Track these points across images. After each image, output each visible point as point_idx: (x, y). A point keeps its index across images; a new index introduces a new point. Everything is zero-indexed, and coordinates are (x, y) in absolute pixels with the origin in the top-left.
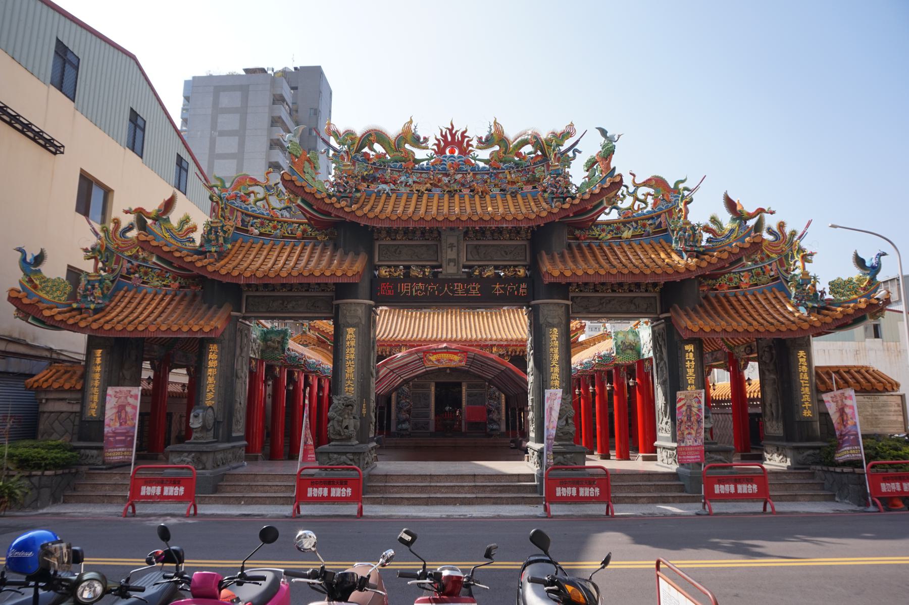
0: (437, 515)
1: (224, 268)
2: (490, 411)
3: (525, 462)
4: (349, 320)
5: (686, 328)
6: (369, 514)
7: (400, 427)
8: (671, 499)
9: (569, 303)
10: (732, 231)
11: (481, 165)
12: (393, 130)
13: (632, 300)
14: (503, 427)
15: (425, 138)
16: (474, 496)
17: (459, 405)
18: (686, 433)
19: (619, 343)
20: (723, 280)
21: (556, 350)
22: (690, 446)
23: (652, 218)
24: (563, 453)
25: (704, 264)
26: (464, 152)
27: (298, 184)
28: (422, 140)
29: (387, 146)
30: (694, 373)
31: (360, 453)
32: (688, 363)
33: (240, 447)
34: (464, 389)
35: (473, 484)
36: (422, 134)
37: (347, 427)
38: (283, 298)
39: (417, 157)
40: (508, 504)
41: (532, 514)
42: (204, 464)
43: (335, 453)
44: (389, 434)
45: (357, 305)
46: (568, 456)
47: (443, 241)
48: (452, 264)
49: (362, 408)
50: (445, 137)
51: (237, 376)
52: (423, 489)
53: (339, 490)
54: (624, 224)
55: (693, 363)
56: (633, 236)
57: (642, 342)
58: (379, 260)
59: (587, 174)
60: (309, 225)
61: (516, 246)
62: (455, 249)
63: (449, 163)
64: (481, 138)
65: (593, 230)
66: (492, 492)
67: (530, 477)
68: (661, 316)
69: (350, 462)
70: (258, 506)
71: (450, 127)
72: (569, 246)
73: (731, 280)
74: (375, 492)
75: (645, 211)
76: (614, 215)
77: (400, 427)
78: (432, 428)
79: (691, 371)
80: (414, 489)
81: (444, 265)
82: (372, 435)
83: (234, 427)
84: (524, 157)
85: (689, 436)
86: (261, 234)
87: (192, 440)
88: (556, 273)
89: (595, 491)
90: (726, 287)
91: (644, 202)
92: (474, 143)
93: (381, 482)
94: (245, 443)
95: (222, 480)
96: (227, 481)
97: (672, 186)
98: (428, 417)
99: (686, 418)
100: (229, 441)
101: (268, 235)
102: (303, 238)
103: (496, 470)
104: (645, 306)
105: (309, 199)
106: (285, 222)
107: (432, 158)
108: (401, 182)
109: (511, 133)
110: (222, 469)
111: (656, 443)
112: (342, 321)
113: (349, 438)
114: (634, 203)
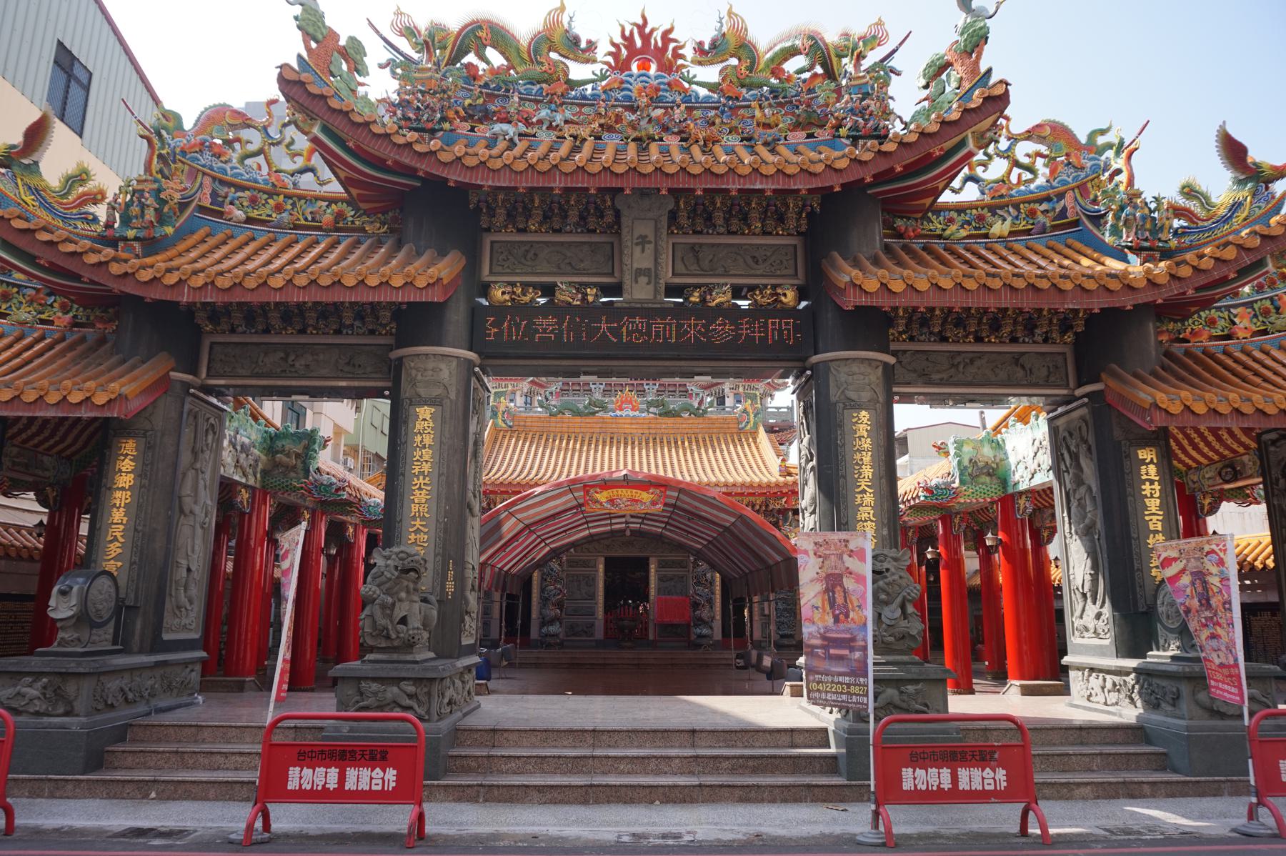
1: (150, 268)
2: (696, 605)
4: (422, 391)
6: (444, 830)
7: (544, 630)
8: (1147, 789)
10: (1236, 206)
11: (703, 92)
12: (524, 24)
13: (1017, 359)
14: (718, 635)
15: (589, 42)
16: (693, 781)
17: (646, 598)
19: (966, 462)
20: (1195, 323)
21: (867, 458)
23: (1048, 199)
25: (1185, 272)
26: (667, 68)
27: (313, 89)
28: (583, 45)
29: (514, 55)
30: (1161, 507)
31: (432, 680)
32: (1147, 486)
33: (186, 664)
34: (653, 568)
35: (689, 752)
36: (584, 33)
37: (403, 621)
40: (773, 801)
42: (70, 703)
43: (374, 679)
44: (527, 643)
45: (441, 362)
46: (911, 688)
47: (625, 231)
50: (629, 40)
51: (182, 511)
52: (576, 765)
53: (365, 773)
54: (993, 209)
55: (1157, 487)
56: (1011, 233)
57: (1012, 460)
58: (491, 273)
61: (777, 248)
62: (650, 248)
63: (637, 86)
64: (701, 43)
65: (930, 221)
66: (733, 771)
67: (819, 736)
68: (1078, 392)
69: (408, 702)
71: (640, 22)
72: (887, 249)
73: (1212, 322)
74: (466, 771)
75: (1032, 186)
76: (971, 193)
78: (599, 633)
79: (1153, 504)
80: (558, 764)
81: (627, 286)
82: (467, 641)
83: (168, 619)
84: (789, 79)
85: (1214, 643)
86: (249, 220)
87: (54, 648)
88: (872, 285)
89: (996, 777)
90: (1205, 336)
91: (1030, 169)
92: (688, 52)
93: (481, 745)
94: (204, 654)
95: (122, 739)
96: (134, 741)
97: (1083, 140)
98: (592, 614)
99: (1195, 603)
100: (153, 650)
101: (263, 222)
102: (337, 230)
103: (739, 720)
104: (1044, 372)
105: (338, 123)
106: (300, 197)
107: (603, 77)
108: (540, 122)
109: (766, 36)
110: (122, 715)
111: (1066, 660)
112: (406, 391)
113: (409, 645)
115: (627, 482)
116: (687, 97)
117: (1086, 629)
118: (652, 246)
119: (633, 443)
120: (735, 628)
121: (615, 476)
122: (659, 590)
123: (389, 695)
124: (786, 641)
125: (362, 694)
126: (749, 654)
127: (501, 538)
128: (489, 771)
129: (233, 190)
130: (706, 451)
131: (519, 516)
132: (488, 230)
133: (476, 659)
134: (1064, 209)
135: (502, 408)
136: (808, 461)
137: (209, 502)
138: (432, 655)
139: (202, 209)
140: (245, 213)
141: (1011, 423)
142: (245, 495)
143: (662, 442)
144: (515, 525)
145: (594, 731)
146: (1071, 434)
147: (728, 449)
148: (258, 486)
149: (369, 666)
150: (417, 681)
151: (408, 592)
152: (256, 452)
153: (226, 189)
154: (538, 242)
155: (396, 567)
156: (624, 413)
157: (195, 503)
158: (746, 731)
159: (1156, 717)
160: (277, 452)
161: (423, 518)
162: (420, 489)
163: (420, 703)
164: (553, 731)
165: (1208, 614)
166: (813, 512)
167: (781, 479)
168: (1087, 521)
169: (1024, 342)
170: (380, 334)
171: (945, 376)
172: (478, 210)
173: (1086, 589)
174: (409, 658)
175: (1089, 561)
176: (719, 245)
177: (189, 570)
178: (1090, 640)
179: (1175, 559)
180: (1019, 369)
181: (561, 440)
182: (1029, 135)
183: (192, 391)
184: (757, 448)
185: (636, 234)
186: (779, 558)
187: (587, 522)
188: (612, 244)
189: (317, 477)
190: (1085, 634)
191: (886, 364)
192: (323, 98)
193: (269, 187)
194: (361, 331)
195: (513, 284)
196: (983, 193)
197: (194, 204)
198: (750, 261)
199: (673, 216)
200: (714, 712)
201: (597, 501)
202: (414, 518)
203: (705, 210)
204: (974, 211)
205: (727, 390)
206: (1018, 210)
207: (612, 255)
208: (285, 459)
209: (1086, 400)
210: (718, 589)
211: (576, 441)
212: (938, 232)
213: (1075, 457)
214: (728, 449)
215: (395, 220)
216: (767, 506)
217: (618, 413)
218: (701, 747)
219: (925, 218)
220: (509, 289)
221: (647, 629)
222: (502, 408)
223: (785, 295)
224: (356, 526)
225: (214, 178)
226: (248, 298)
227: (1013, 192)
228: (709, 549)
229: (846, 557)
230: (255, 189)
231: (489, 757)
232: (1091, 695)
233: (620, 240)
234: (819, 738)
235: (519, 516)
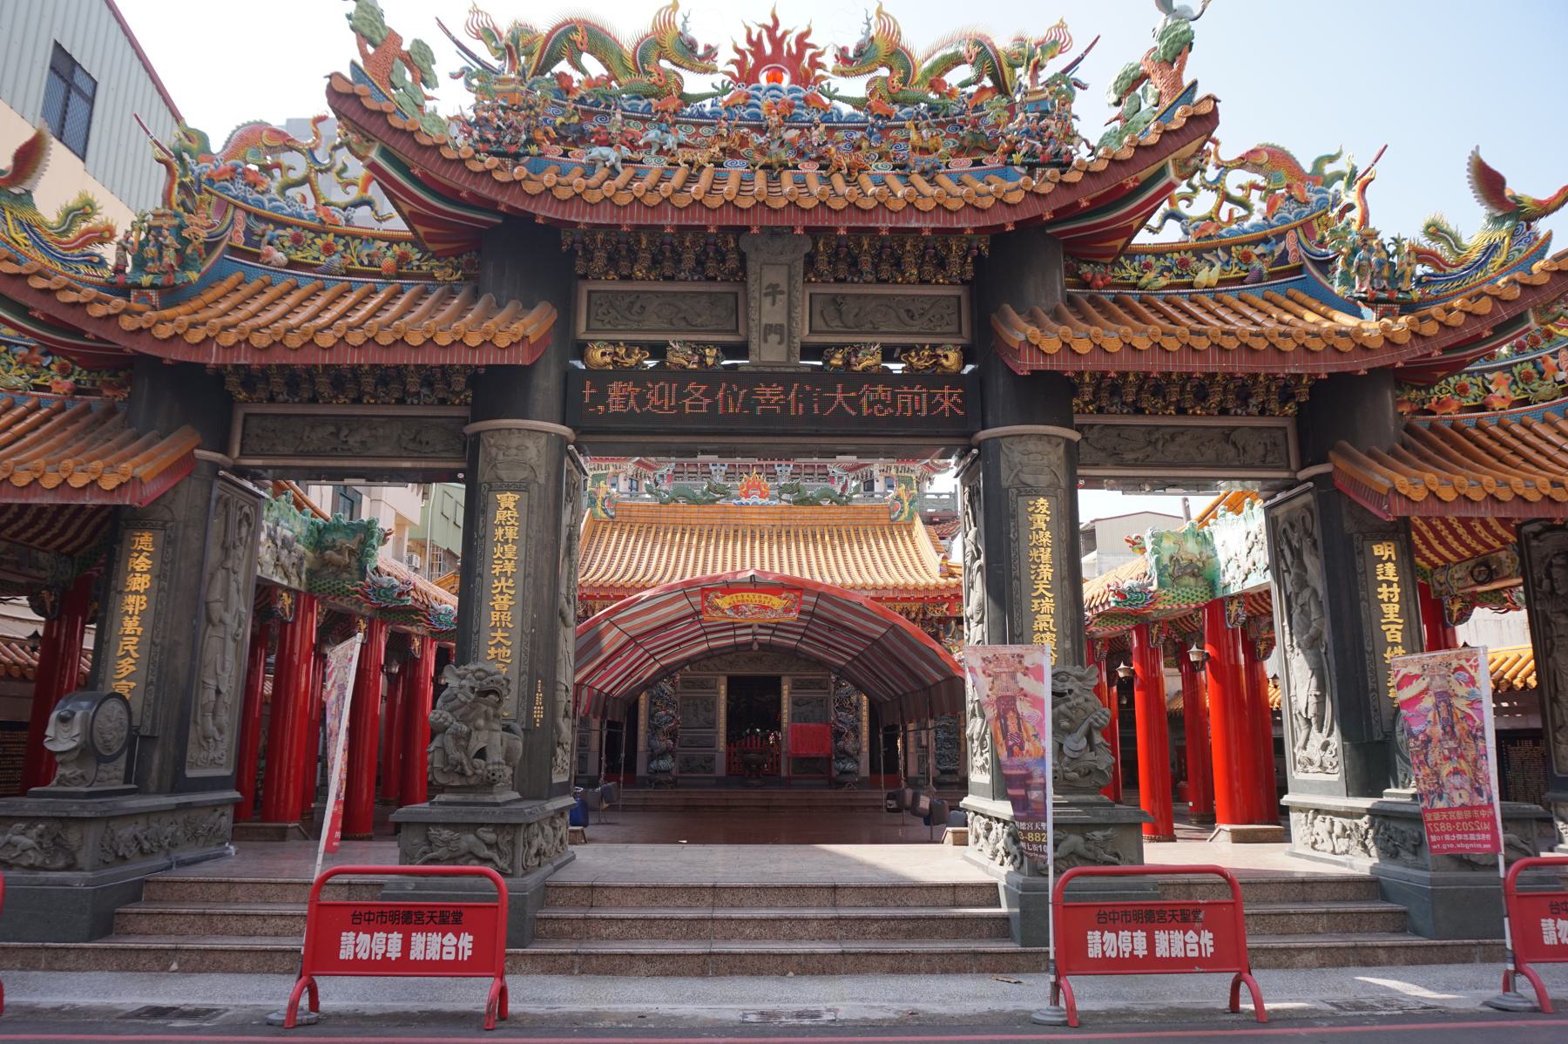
0: (729, 1012)
2: (839, 735)
3: (948, 847)
4: (504, 474)
5: (1395, 491)
6: (532, 1008)
7: (653, 765)
8: (1382, 955)
9: (1075, 436)
10: (1491, 249)
11: (846, 109)
13: (1227, 435)
14: (865, 770)
15: (708, 48)
16: (835, 948)
17: (777, 726)
18: (1446, 769)
19: (1166, 561)
20: (1443, 390)
21: (1046, 556)
22: (1463, 807)
24: (1082, 828)
25: (1430, 329)
26: (803, 79)
27: (371, 104)
28: (701, 51)
29: (615, 63)
30: (1400, 615)
31: (516, 826)
32: (1384, 589)
33: (215, 806)
34: (785, 689)
35: (829, 913)
37: (481, 754)
38: (339, 421)
39: (688, 89)
40: (932, 972)
41: (1009, 1006)
42: (71, 855)
43: (446, 825)
44: (632, 781)
45: (528, 438)
46: (1098, 834)
47: (751, 279)
49: (531, 702)
50: (757, 45)
51: (209, 620)
52: (694, 928)
53: (435, 939)
54: (1198, 253)
55: (1396, 589)
56: (1221, 282)
57: (1222, 557)
58: (589, 329)
59: (1117, 111)
60: (414, 245)
63: (765, 101)
65: (1122, 267)
66: (883, 935)
67: (988, 893)
68: (1301, 475)
69: (486, 853)
70: (217, 979)
71: (770, 23)
72: (1071, 301)
73: (1462, 390)
74: (557, 936)
75: (1246, 225)
76: (1172, 233)
77: (653, 765)
78: (720, 768)
79: (1392, 610)
80: (668, 927)
82: (559, 778)
83: (193, 752)
84: (951, 93)
85: (1457, 780)
88: (1052, 345)
89: (1200, 942)
90: (1455, 407)
91: (1244, 204)
92: (829, 60)
93: (577, 905)
94: (237, 795)
95: (136, 898)
96: (150, 900)
98: (711, 745)
99: (1439, 729)
100: (174, 790)
101: (309, 267)
102: (400, 276)
104: (1260, 450)
105: (401, 147)
106: (354, 236)
107: (725, 91)
108: (648, 145)
110: (136, 869)
112: (484, 474)
113: (488, 784)
114: (1220, 206)
115: (754, 585)
116: (828, 116)
117: (1311, 762)
119: (762, 537)
120: (886, 762)
121: (739, 577)
123: (464, 845)
124: (947, 778)
125: (430, 843)
127: (600, 653)
130: (851, 546)
131: (622, 626)
132: (585, 277)
133: (570, 801)
134: (1285, 253)
135: (602, 494)
136: (974, 559)
137: (243, 609)
138: (516, 795)
139: (233, 250)
140: (287, 255)
143: (797, 536)
144: (618, 637)
145: (714, 887)
146: (1292, 526)
147: (877, 544)
148: (303, 589)
149: (438, 809)
150: (498, 827)
151: (487, 719)
152: (301, 548)
153: (263, 226)
155: (472, 689)
156: (750, 501)
157: (226, 610)
158: (899, 887)
159: (1394, 868)
160: (327, 548)
162: (501, 593)
163: (501, 854)
164: (663, 888)
165: (1452, 744)
166: (981, 622)
167: (942, 581)
168: (1312, 631)
170: (453, 404)
171: (1140, 455)
172: (572, 252)
173: (1310, 714)
174: (488, 799)
175: (1314, 680)
176: (866, 296)
177: (218, 692)
178: (1314, 776)
179: (1417, 677)
180: (1230, 447)
181: (674, 534)
182: (1243, 162)
183: (222, 473)
184: (913, 543)
185: (765, 283)
186: (939, 678)
187: (706, 634)
189: (375, 578)
190: (1309, 768)
191: (1069, 442)
192: (382, 114)
193: (316, 224)
195: (615, 343)
196: (1186, 233)
197: (223, 245)
198: (904, 316)
199: (810, 261)
201: (718, 608)
202: (494, 629)
203: (849, 253)
204: (1176, 255)
205: (876, 473)
207: (736, 308)
208: (336, 557)
209: (1310, 484)
211: (692, 535)
212: (1132, 280)
213: (1297, 554)
214: (877, 544)
215: (470, 264)
216: (925, 614)
217: (744, 500)
218: (845, 907)
220: (610, 349)
221: (778, 764)
222: (602, 494)
223: (946, 357)
224: (423, 638)
225: (248, 213)
226: (291, 359)
227: (1223, 232)
229: (1019, 676)
231: (585, 919)
232: (1315, 842)
235: (622, 626)
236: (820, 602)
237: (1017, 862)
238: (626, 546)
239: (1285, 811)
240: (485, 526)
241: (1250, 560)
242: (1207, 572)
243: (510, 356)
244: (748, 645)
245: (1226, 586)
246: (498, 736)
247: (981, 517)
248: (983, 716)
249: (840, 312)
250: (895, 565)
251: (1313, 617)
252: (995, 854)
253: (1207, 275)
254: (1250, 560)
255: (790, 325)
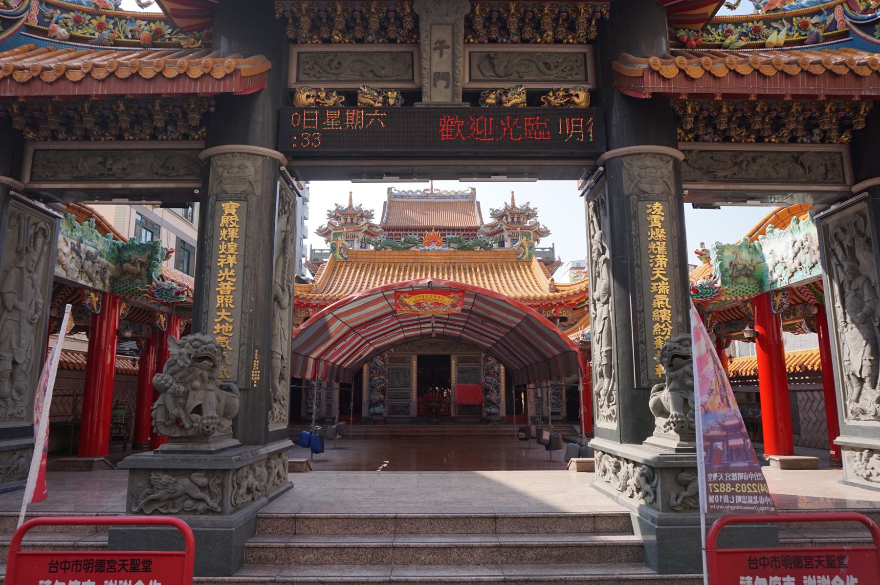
2: (487, 391)
4: (228, 188)
7: (371, 410)
13: (796, 158)
14: (503, 413)
17: (448, 385)
19: (727, 265)
23: (819, 13)
31: (225, 471)
37: (198, 410)
43: (165, 471)
45: (250, 158)
47: (423, 35)
48: (441, 84)
49: (250, 367)
54: (768, 22)
56: (787, 44)
57: (769, 262)
60: (166, 23)
62: (447, 52)
65: (709, 33)
66: (537, 561)
67: (622, 523)
68: (855, 189)
69: (199, 494)
74: (263, 562)
77: (371, 410)
78: (413, 412)
104: (822, 170)
111: (838, 440)
113: (204, 435)
115: (431, 289)
117: (864, 412)
118: (449, 51)
119: (438, 270)
120: (516, 410)
121: (421, 283)
122: (458, 379)
123: (180, 487)
125: (152, 486)
126: (529, 428)
127: (329, 338)
128: (287, 563)
129: (59, 11)
130: (493, 275)
131: (344, 319)
132: (295, 41)
134: (834, 22)
135: (339, 245)
136: (599, 255)
137: (41, 300)
138: (236, 442)
139: (30, 29)
140: (68, 31)
141: (768, 229)
142: (94, 299)
143: (459, 269)
144: (341, 327)
145: (395, 518)
146: (844, 230)
147: (509, 273)
148: (107, 290)
149: (159, 457)
150: (209, 472)
151: (202, 380)
152: (104, 260)
153: (52, 11)
154: (342, 52)
155: (189, 355)
156: (430, 248)
157: (20, 299)
158: (549, 517)
160: (125, 262)
161: (228, 309)
162: (225, 281)
163: (212, 495)
164: (354, 518)
166: (607, 302)
167: (551, 294)
168: (865, 310)
169: (802, 142)
170: (193, 139)
171: (729, 173)
172: (284, 20)
173: (864, 375)
174: (203, 447)
175: (868, 348)
176: (513, 53)
177: (14, 363)
178: (865, 422)
180: (798, 167)
181: (384, 269)
183: (12, 193)
184: (531, 272)
185: (434, 39)
186: (557, 352)
187: (402, 327)
188: (412, 53)
189: (160, 282)
190: (862, 417)
191: (676, 160)
193: (92, 8)
194: (175, 136)
195: (319, 90)
196: (758, 8)
197: (20, 24)
198: (542, 67)
199: (469, 27)
200: (513, 492)
201: (406, 305)
202: (219, 309)
203: (499, 18)
204: (750, 24)
205: (506, 237)
206: (791, 22)
207: (412, 63)
208: (131, 267)
209: (866, 194)
210: (503, 378)
211: (395, 269)
212: (717, 42)
213: (851, 253)
214: (509, 273)
217: (427, 248)
218: (504, 534)
219: (704, 29)
220: (313, 93)
221: (449, 408)
222: (339, 245)
223: (577, 96)
226: (48, 91)
227: (786, 7)
228: (501, 344)
230: (79, 10)
231: (286, 548)
232: (871, 475)
233: (419, 50)
234: (621, 524)
235: (344, 319)
236: (477, 302)
237: (650, 499)
238: (354, 276)
239: (838, 449)
240: (213, 229)
241: (796, 262)
242: (757, 273)
243: (225, 85)
244: (429, 335)
245: (774, 283)
246: (212, 396)
247: (606, 221)
248: (609, 376)
249: (493, 65)
250: (521, 286)
251: (866, 299)
252: (624, 488)
253: (776, 37)
254: (796, 262)
255: (454, 72)
